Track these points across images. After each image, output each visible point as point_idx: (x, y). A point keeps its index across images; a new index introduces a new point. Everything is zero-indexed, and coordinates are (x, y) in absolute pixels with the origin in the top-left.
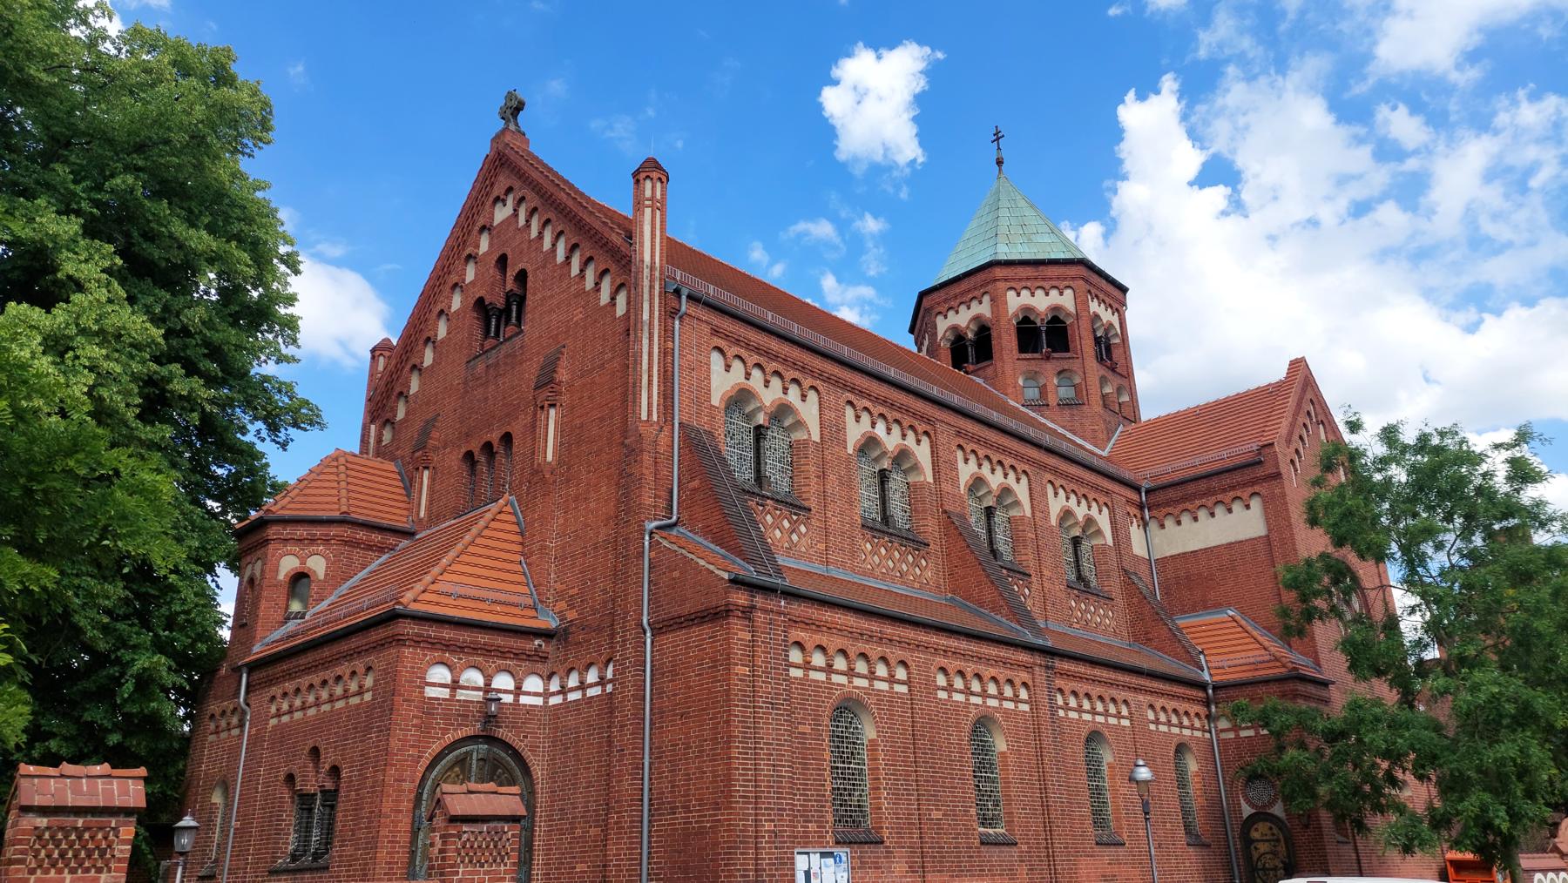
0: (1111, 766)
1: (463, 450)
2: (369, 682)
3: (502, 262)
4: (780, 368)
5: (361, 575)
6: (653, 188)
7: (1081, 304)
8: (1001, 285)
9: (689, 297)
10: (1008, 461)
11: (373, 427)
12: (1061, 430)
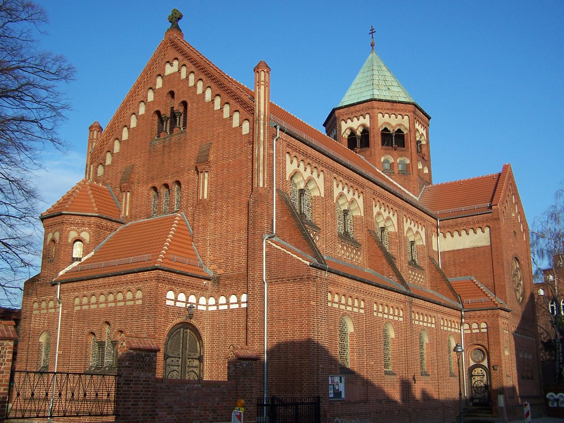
0: (427, 344)
1: (150, 185)
2: (139, 294)
4: (311, 162)
5: (104, 242)
6: (265, 76)
7: (412, 124)
8: (376, 111)
9: (280, 130)
10: (391, 206)
11: (92, 166)
12: (399, 186)
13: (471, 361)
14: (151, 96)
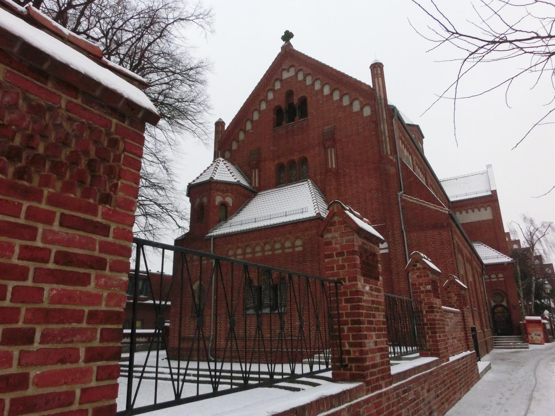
2: (299, 242)
3: (290, 94)
13: (492, 302)
14: (271, 96)
